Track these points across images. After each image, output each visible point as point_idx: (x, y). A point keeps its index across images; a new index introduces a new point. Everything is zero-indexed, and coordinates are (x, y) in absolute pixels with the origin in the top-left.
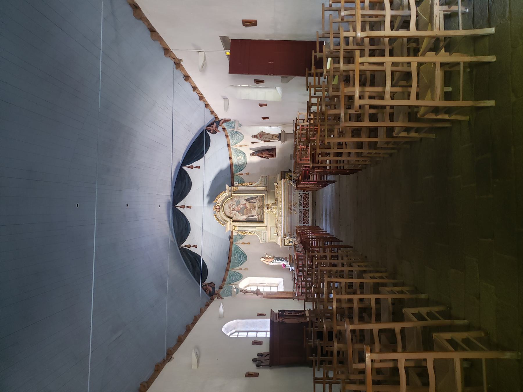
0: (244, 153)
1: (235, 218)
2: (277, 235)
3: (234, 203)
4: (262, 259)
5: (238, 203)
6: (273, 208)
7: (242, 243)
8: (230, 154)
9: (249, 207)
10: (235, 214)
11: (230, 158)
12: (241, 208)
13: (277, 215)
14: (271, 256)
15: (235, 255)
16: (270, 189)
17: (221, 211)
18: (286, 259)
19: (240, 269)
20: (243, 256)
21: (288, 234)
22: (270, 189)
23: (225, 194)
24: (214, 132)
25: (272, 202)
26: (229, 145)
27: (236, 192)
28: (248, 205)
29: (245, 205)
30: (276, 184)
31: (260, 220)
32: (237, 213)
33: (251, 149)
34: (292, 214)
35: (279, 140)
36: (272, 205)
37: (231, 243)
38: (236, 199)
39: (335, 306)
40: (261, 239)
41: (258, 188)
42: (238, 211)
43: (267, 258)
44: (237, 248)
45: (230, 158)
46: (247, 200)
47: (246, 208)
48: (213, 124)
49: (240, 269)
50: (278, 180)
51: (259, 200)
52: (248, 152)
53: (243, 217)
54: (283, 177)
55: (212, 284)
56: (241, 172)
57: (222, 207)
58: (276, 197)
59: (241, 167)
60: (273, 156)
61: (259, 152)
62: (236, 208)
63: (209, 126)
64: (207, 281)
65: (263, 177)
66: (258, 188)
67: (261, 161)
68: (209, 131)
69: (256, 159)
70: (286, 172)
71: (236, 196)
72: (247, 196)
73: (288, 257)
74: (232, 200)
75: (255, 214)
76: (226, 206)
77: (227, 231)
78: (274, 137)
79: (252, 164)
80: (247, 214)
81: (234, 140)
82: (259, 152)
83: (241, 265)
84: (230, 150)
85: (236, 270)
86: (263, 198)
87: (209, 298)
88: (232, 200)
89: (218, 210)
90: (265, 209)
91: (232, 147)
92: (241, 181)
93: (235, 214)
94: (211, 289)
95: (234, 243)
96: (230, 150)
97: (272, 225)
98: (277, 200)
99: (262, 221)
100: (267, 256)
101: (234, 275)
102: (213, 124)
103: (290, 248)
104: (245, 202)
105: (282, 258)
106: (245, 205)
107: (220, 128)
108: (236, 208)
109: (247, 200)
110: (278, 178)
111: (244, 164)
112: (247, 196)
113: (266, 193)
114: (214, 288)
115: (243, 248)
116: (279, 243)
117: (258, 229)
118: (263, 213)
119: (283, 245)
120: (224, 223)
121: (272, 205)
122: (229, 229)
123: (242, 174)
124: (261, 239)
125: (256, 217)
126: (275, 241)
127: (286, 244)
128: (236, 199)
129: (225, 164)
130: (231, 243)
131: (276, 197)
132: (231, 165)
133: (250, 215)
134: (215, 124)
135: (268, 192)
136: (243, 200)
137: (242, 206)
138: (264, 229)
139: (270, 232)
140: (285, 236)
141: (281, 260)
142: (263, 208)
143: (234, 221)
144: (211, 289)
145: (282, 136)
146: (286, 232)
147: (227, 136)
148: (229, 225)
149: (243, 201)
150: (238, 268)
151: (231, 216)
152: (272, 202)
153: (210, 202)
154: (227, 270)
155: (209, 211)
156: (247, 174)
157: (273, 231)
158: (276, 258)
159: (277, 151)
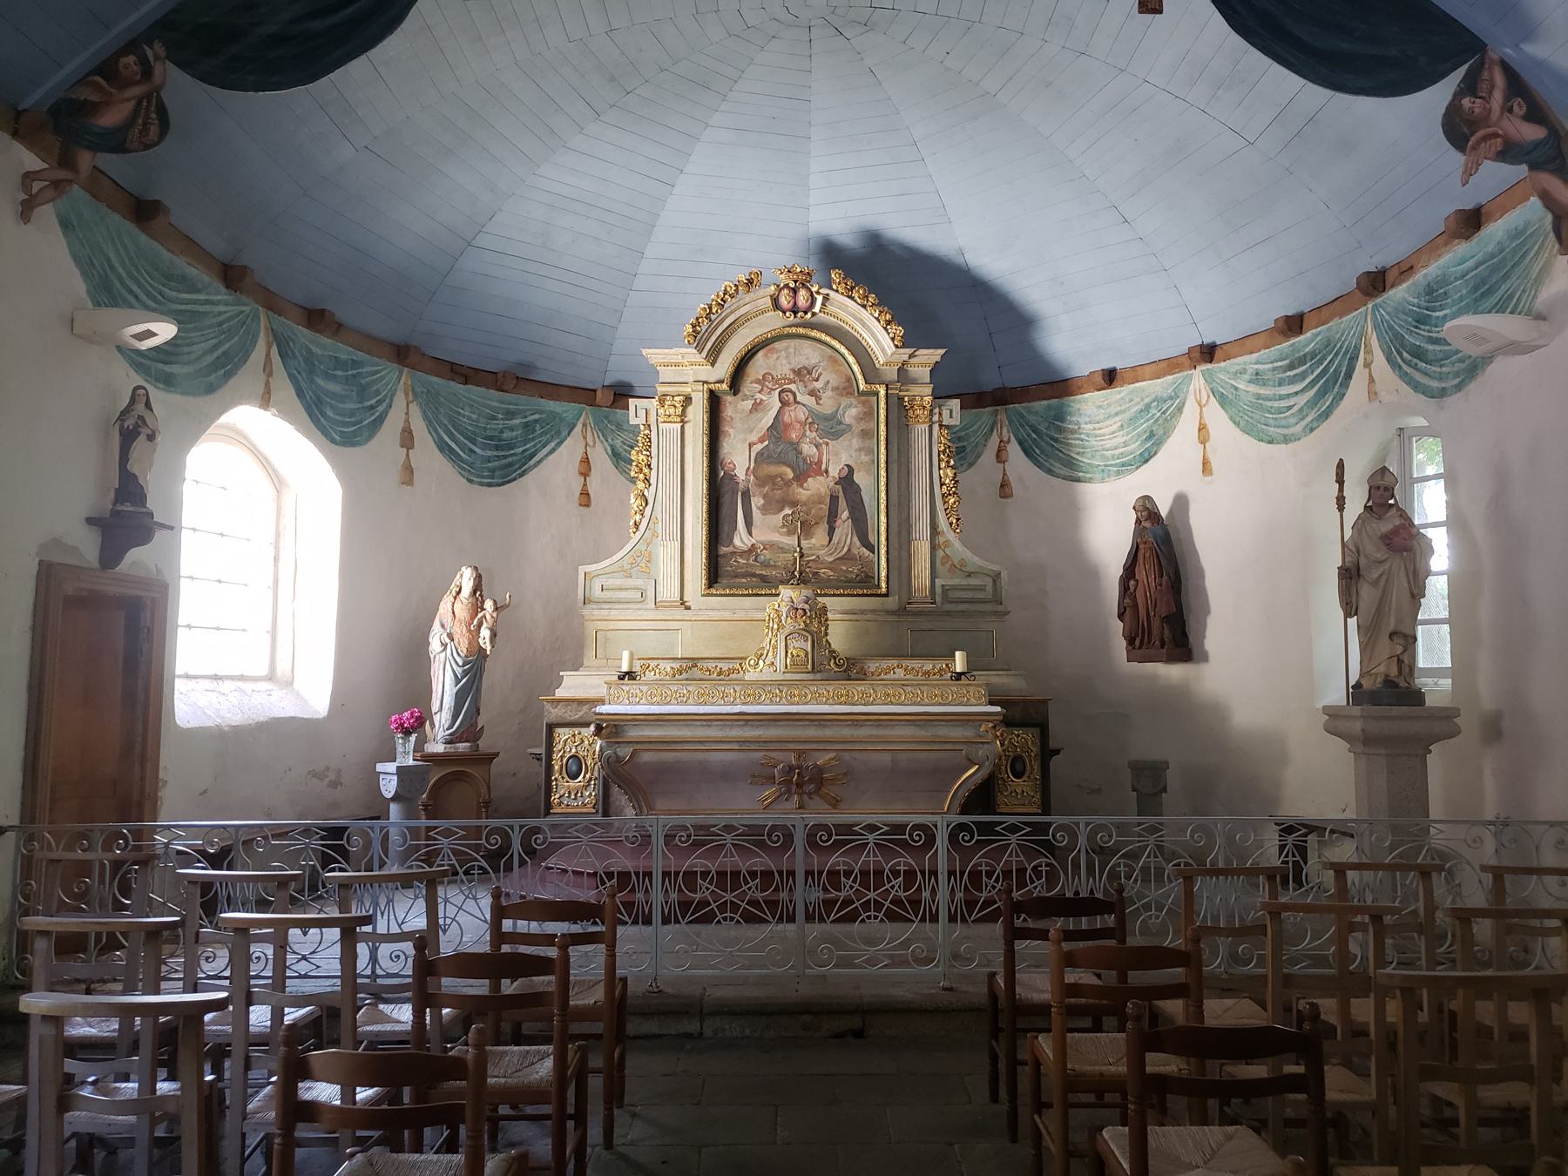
0: (1146, 458)
1: (734, 409)
2: (630, 675)
3: (828, 404)
4: (466, 579)
5: (831, 428)
6: (802, 645)
7: (586, 461)
8: (1136, 374)
9: (802, 493)
10: (757, 406)
11: (1110, 377)
12: (795, 447)
13: (751, 675)
14: (485, 633)
15: (510, 415)
16: (919, 625)
17: (774, 322)
18: (468, 731)
19: (407, 439)
20: (499, 461)
21: (625, 752)
22: (919, 625)
23: (880, 340)
24: (1458, 129)
25: (839, 636)
26: (1208, 353)
27: (899, 413)
28: (817, 486)
29: (817, 469)
30: (960, 662)
31: (726, 567)
32: (768, 420)
33: (1181, 502)
34: (762, 776)
35: (1357, 693)
36: (818, 639)
37: (585, 395)
38: (851, 414)
39: (957, 544)
40: (600, 575)
41: (922, 549)
42: (777, 429)
43: (477, 607)
44: (556, 431)
45: (1110, 377)
46: (847, 481)
47: (801, 477)
48: (1536, 114)
49: (407, 439)
50: (983, 677)
51: (848, 557)
52: (1160, 481)
53: (739, 457)
54: (1022, 714)
55: (155, 119)
56: (1014, 449)
57: (805, 325)
58: (872, 666)
59: (1053, 451)
60: (1141, 642)
61: (1161, 548)
62: (796, 414)
63: (1517, 86)
64: (181, 88)
65: (996, 577)
66: (922, 549)
67: (1091, 573)
68: (1470, 86)
69: (1108, 535)
70: (1043, 728)
71: (870, 414)
72: (873, 486)
73: (484, 744)
74: (847, 388)
75: (760, 532)
76: (808, 354)
77: (654, 355)
78: (1385, 648)
79: (1071, 516)
80: (762, 481)
81: (1257, 378)
82: (1161, 548)
83: (443, 447)
84: (1170, 366)
85: (403, 411)
86: (863, 583)
87: (36, 97)
88: (847, 388)
89: (785, 301)
90: (786, 592)
91: (1197, 379)
92: (961, 451)
93: (757, 406)
94: (110, 119)
95: (587, 414)
96: (1170, 366)
97: (685, 643)
98: (849, 670)
99: (715, 574)
100: (489, 605)
101: (363, 392)
102: (1536, 114)
103: (538, 757)
104: (835, 472)
105: (476, 711)
106: (817, 469)
107: (1496, 175)
108: (796, 414)
109: (847, 481)
110: (1000, 679)
111: (1070, 463)
112: (873, 486)
113: (892, 602)
114: (115, 142)
115: (557, 468)
116: (573, 685)
117: (666, 554)
118: (763, 583)
119: (554, 713)
120: (707, 335)
121: (818, 639)
122: (666, 374)
123: (1000, 456)
124: (600, 575)
125: (741, 539)
126: (589, 659)
127: (562, 734)
128: (851, 414)
129: (1069, 343)
130: (585, 395)
131: (872, 666)
132: (1060, 387)
133: (757, 502)
134: (1532, 133)
135: (901, 611)
136: (845, 459)
137: (808, 449)
138: (669, 591)
139: (655, 620)
140: (610, 729)
141: (460, 698)
142: (803, 581)
143: (715, 403)
144: (110, 119)
145: (1395, 719)
146: (634, 733)
147: (1293, 325)
148: (689, 374)
149: (839, 456)
150: (419, 426)
151: (749, 386)
152: (839, 636)
153: (831, 255)
154: (402, 354)
155: (775, 249)
156: (1004, 485)
157: (651, 644)
158: (475, 667)
159: (1173, 672)
